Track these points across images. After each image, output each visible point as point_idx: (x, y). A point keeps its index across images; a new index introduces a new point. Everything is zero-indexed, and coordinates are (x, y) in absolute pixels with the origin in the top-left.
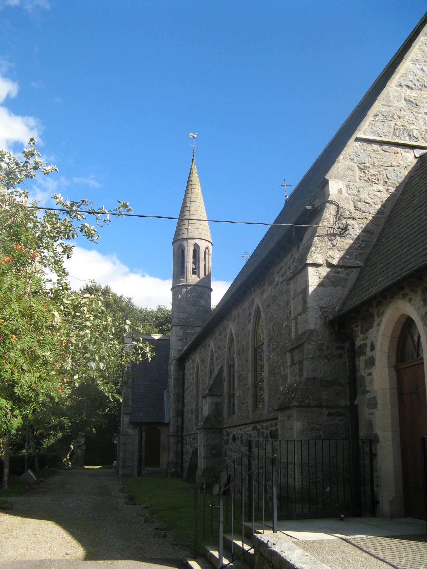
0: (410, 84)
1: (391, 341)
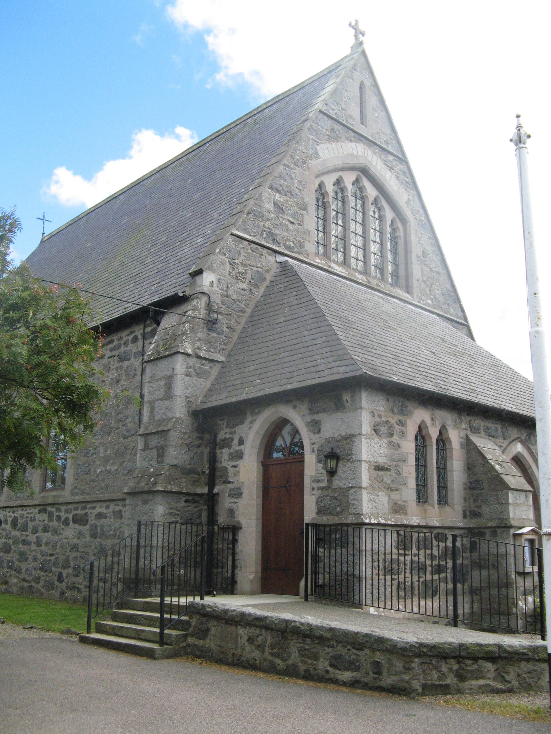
0: (280, 189)
1: (263, 439)
